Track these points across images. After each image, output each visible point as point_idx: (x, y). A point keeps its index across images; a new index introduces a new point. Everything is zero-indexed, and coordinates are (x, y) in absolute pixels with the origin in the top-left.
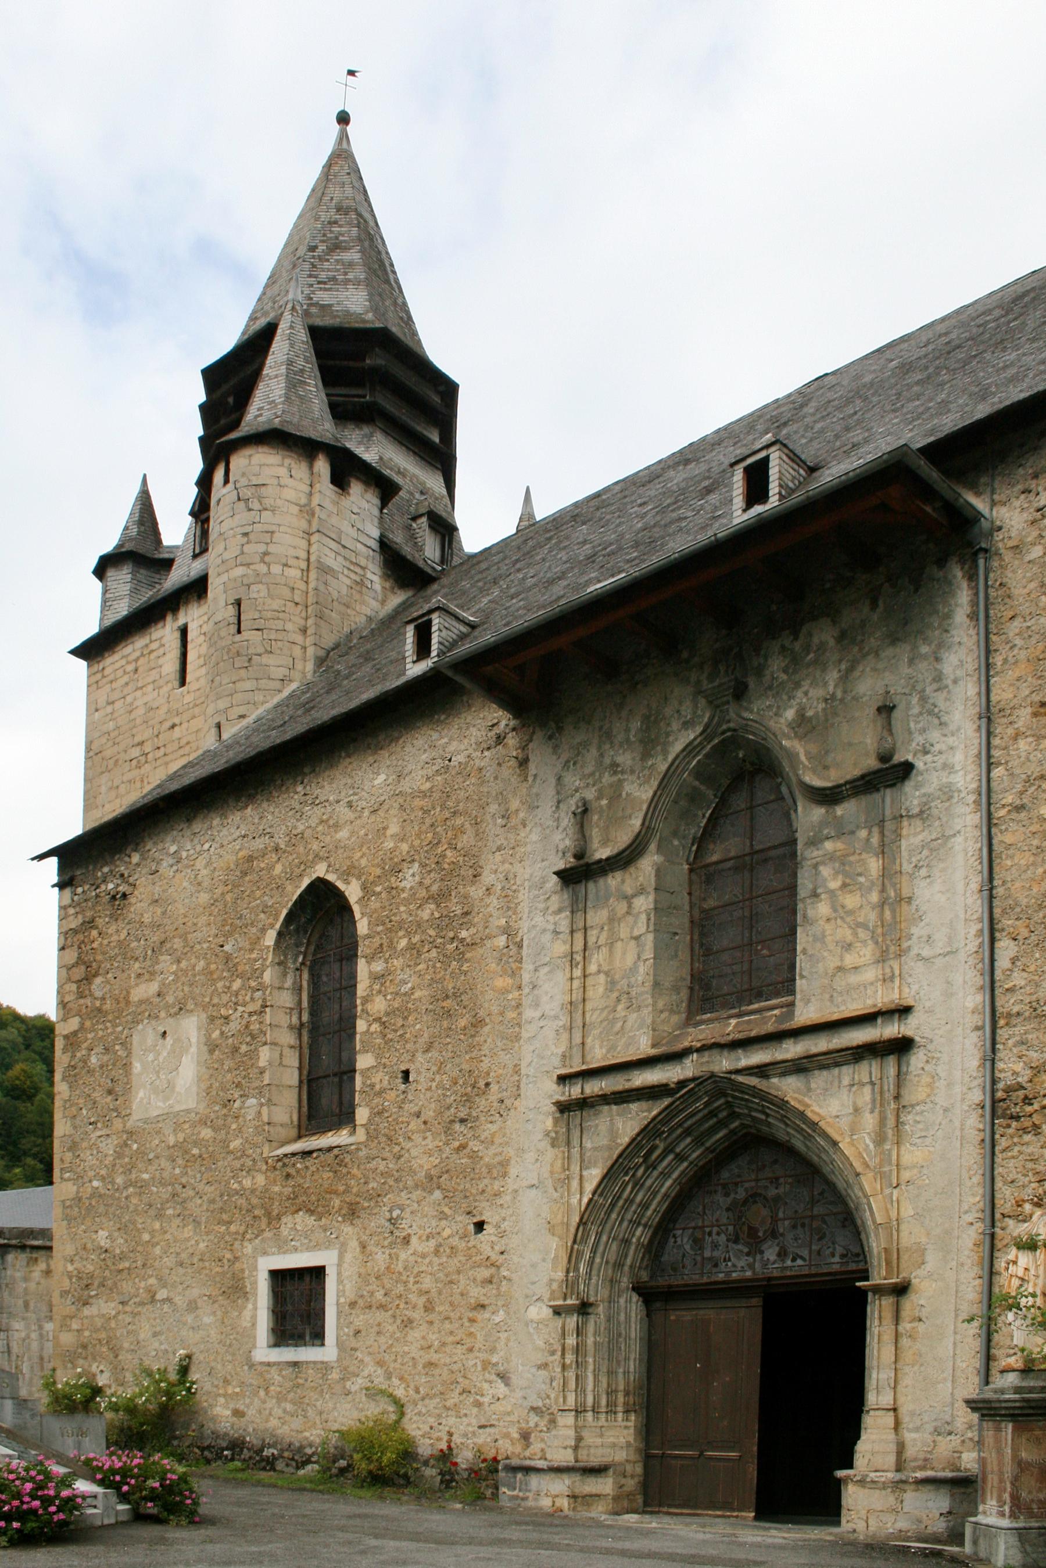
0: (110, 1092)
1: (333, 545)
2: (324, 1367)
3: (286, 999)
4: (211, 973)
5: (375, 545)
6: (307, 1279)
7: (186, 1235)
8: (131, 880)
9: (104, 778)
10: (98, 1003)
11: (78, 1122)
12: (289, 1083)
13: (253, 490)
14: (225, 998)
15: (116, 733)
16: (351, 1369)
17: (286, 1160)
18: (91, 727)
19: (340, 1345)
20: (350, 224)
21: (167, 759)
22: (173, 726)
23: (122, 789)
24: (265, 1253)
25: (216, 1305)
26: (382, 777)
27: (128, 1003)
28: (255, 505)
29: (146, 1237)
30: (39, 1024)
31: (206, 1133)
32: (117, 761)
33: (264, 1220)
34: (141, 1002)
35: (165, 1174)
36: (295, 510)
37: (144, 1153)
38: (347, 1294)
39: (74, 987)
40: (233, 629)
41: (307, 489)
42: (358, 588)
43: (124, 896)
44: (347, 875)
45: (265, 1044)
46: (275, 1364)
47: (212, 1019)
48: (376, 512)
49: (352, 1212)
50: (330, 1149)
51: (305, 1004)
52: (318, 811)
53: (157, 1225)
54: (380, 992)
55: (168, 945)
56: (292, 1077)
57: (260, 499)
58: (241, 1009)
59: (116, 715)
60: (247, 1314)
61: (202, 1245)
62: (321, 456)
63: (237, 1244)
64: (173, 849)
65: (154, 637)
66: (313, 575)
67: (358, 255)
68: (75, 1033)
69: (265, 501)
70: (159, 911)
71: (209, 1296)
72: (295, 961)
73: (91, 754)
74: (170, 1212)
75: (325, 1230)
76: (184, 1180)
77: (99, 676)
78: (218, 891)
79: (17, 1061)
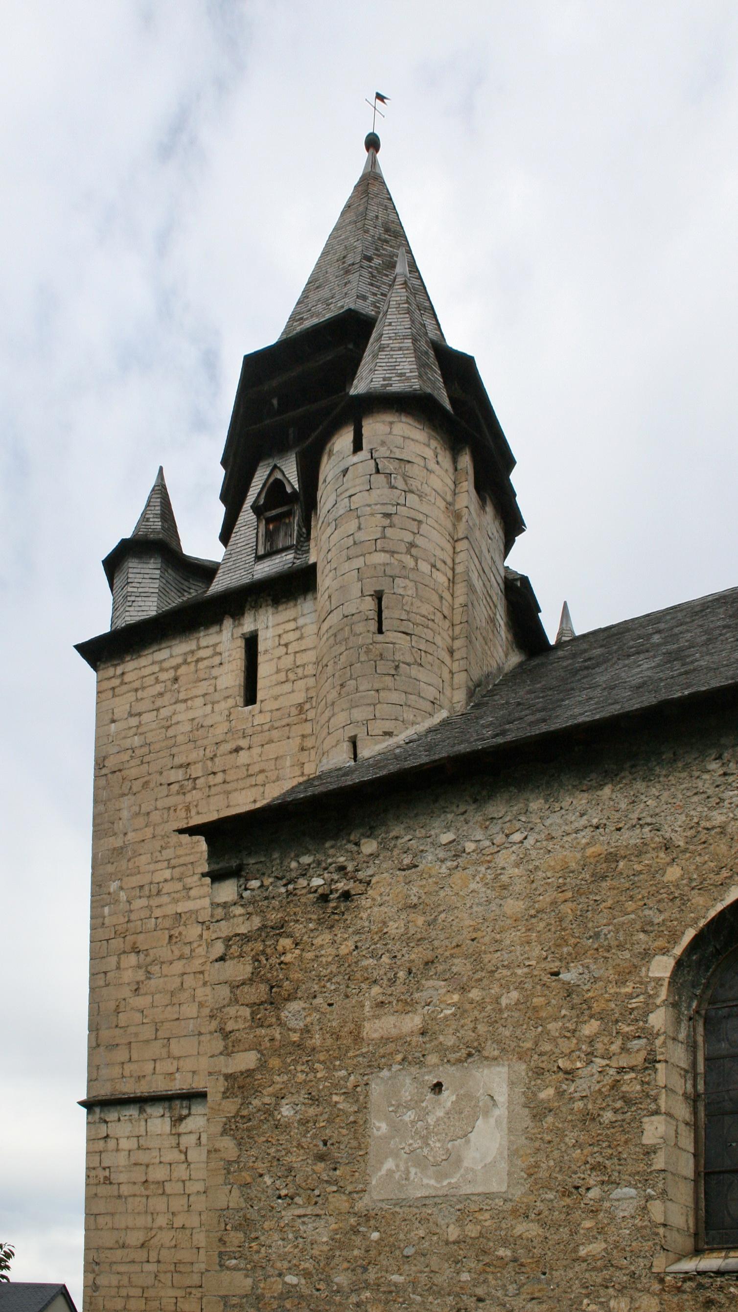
0: (321, 1158)
3: (679, 1055)
4: (535, 1009)
5: (502, 586)
8: (361, 875)
9: (126, 802)
10: (295, 1037)
11: (253, 1193)
14: (565, 1046)
15: (145, 750)
17: (706, 1281)
18: (102, 741)
21: (228, 787)
22: (237, 750)
23: (156, 817)
27: (357, 1038)
28: (400, 483)
32: (146, 783)
34: (386, 1040)
35: (438, 1279)
36: (442, 505)
37: (393, 1247)
39: (246, 1012)
40: (373, 626)
41: (452, 486)
43: (346, 896)
45: (657, 1112)
47: (539, 1072)
51: (701, 1068)
57: (406, 477)
64: (446, 838)
68: (249, 1073)
69: (411, 481)
72: (689, 1006)
73: (104, 771)
76: (480, 1291)
77: (116, 682)
78: (547, 898)
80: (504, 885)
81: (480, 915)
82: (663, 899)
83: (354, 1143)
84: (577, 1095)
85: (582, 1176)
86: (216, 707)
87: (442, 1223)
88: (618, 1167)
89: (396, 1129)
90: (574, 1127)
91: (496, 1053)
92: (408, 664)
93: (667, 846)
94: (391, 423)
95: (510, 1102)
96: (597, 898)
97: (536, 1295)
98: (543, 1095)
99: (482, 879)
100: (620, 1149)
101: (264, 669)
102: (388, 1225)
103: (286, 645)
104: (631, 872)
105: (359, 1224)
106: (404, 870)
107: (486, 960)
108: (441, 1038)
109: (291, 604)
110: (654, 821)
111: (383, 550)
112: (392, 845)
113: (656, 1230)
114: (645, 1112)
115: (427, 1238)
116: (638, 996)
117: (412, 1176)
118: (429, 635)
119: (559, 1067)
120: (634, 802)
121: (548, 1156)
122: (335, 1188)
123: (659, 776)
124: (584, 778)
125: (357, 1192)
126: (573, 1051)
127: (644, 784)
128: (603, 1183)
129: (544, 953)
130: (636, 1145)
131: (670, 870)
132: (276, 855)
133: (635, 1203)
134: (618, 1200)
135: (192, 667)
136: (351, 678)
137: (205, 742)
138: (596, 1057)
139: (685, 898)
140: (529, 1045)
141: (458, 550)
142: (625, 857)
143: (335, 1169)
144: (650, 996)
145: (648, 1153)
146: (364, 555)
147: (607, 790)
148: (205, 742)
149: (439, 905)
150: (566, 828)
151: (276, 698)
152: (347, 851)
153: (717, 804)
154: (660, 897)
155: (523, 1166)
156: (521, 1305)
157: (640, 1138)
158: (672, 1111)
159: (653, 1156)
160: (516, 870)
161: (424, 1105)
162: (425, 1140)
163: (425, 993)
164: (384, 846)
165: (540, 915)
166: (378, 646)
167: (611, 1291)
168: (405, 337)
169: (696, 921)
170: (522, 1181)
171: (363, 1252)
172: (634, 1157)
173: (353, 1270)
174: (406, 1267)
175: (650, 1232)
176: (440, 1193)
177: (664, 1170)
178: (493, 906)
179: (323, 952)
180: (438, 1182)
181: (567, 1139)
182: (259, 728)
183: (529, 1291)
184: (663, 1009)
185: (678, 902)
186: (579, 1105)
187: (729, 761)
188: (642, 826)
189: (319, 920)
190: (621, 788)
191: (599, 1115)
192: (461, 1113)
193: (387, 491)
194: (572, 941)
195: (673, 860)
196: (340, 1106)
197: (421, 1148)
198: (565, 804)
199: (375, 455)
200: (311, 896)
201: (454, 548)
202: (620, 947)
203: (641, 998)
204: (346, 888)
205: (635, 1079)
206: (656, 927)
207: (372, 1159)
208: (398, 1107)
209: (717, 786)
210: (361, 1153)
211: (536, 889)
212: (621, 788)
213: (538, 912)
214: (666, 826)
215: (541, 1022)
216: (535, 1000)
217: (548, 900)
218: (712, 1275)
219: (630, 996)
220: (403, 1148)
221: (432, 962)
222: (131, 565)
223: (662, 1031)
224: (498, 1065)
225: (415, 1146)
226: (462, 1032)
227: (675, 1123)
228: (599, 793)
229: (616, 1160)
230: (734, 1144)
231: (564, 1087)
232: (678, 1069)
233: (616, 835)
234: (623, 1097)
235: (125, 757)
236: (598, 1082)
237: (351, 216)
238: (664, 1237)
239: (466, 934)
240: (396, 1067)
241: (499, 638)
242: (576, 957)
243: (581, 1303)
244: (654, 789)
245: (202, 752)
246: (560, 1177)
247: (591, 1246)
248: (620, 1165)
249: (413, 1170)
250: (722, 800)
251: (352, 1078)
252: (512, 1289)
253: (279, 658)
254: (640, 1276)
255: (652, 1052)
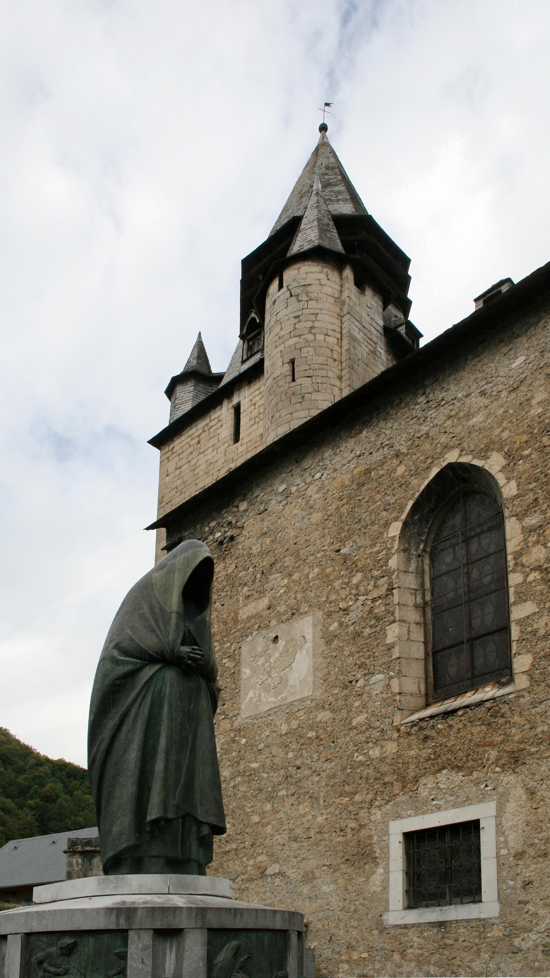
1: (357, 324)
2: (483, 924)
3: (411, 581)
4: (327, 576)
5: (382, 331)
6: (448, 837)
7: (302, 812)
8: (239, 524)
12: (416, 656)
13: (302, 288)
14: (343, 593)
16: (521, 923)
17: (424, 724)
19: (502, 898)
20: (335, 174)
24: (398, 817)
25: (338, 874)
26: (521, 359)
27: (236, 621)
29: (256, 819)
30: (60, 764)
31: (324, 716)
33: (397, 786)
34: (250, 618)
35: (277, 760)
36: (331, 300)
38: (511, 844)
40: (289, 379)
41: (339, 288)
42: (373, 355)
43: (232, 538)
44: (484, 454)
45: (394, 621)
46: (413, 925)
47: (329, 614)
48: (381, 310)
49: (515, 760)
50: (480, 703)
51: (428, 585)
52: (446, 410)
53: (268, 807)
54: (538, 542)
55: (278, 566)
56: (418, 651)
57: (307, 294)
58: (362, 598)
59: (182, 474)
60: (377, 877)
61: (320, 819)
62: (348, 267)
63: (363, 813)
64: (281, 489)
65: (213, 417)
66: (345, 342)
67: (344, 188)
69: (310, 295)
70: (268, 541)
71: (329, 866)
72: (417, 549)
73: (163, 504)
74: (284, 792)
75: (478, 784)
76: (298, 763)
77: (170, 453)
79: (48, 783)
80: (311, 506)
81: (299, 528)
82: (395, 487)
83: (233, 686)
84: (350, 623)
85: (354, 673)
86: (219, 450)
87: (278, 723)
88: (373, 663)
89: (253, 671)
90: (348, 643)
91: (307, 609)
92: (310, 393)
93: (397, 455)
94: (299, 268)
95: (314, 638)
96: (360, 498)
97: (329, 757)
98: (331, 628)
99: (299, 506)
100: (374, 651)
101: (243, 422)
102: (250, 732)
103: (255, 404)
104: (378, 477)
105: (235, 736)
106: (260, 514)
107: (302, 554)
108: (278, 608)
109: (257, 381)
110: (389, 442)
111: (295, 336)
112: (254, 502)
113: (395, 698)
114: (387, 623)
115: (271, 735)
116: (382, 551)
117: (262, 698)
118: (324, 373)
119: (340, 608)
120: (379, 435)
121: (335, 666)
122: (223, 717)
123: (392, 415)
124: (352, 430)
125: (234, 716)
126: (347, 596)
127: (384, 422)
128: (365, 675)
129: (332, 540)
130: (383, 646)
131: (399, 468)
132: (198, 526)
133: (383, 683)
134: (374, 684)
135: (207, 432)
136: (277, 412)
137: (213, 471)
138: (360, 595)
139: (407, 483)
140: (324, 599)
141: (343, 321)
142: (375, 469)
143: (224, 705)
144: (389, 549)
145: (390, 649)
146: (284, 343)
147: (364, 433)
148: (213, 471)
149: (278, 529)
150: (343, 462)
151: (249, 435)
152: (233, 513)
153: (424, 421)
154: (394, 486)
155: (321, 676)
156: (320, 766)
157: (385, 640)
158: (404, 618)
159: (392, 650)
160: (317, 495)
161: (269, 652)
162: (269, 673)
163: (270, 583)
164: (251, 504)
165: (330, 518)
166: (291, 389)
167: (370, 744)
168: (314, 221)
169: (413, 495)
170: (321, 686)
171: (237, 753)
172: (382, 653)
173: (232, 766)
174: (260, 757)
175: (393, 701)
176: (277, 705)
177: (399, 658)
178: (306, 521)
179: (220, 575)
180: (276, 698)
181: (345, 652)
182: (240, 454)
183: (325, 756)
184: (396, 555)
185: (404, 487)
186: (352, 628)
187: (429, 394)
188: (383, 448)
189: (218, 556)
190: (372, 429)
191: (362, 632)
192: (288, 651)
193: (297, 304)
194: (347, 528)
195: (401, 462)
196: (226, 665)
197: (267, 679)
198: (342, 449)
199: (290, 288)
200: (215, 544)
201: (341, 321)
202: (373, 523)
203: (384, 552)
204: (231, 534)
205: (382, 603)
206: (392, 506)
207: (242, 694)
208: (255, 657)
209: (424, 410)
210: (237, 691)
211: (327, 503)
212: (372, 429)
213: (328, 517)
214: (396, 443)
215: (330, 583)
216: (327, 570)
217: (334, 507)
218: (427, 719)
219: (378, 552)
220: (258, 682)
221: (274, 564)
222: (178, 389)
223: (396, 569)
224: (307, 616)
225: (264, 679)
226: (289, 601)
227: (407, 625)
228: (361, 436)
229: (372, 659)
230: (450, 629)
231: (343, 619)
232: (409, 590)
233: (370, 457)
234: (375, 617)
235: (173, 493)
236: (362, 611)
237: (309, 168)
238: (400, 701)
239: (292, 542)
240: (255, 633)
241: (380, 360)
242: (347, 538)
243: (353, 756)
244: (389, 424)
245: (211, 477)
246: (341, 677)
247: (359, 718)
248: (374, 661)
249: (263, 694)
250: (426, 418)
251: (233, 646)
252: (315, 756)
253: (251, 412)
254: (386, 730)
255: (391, 584)
